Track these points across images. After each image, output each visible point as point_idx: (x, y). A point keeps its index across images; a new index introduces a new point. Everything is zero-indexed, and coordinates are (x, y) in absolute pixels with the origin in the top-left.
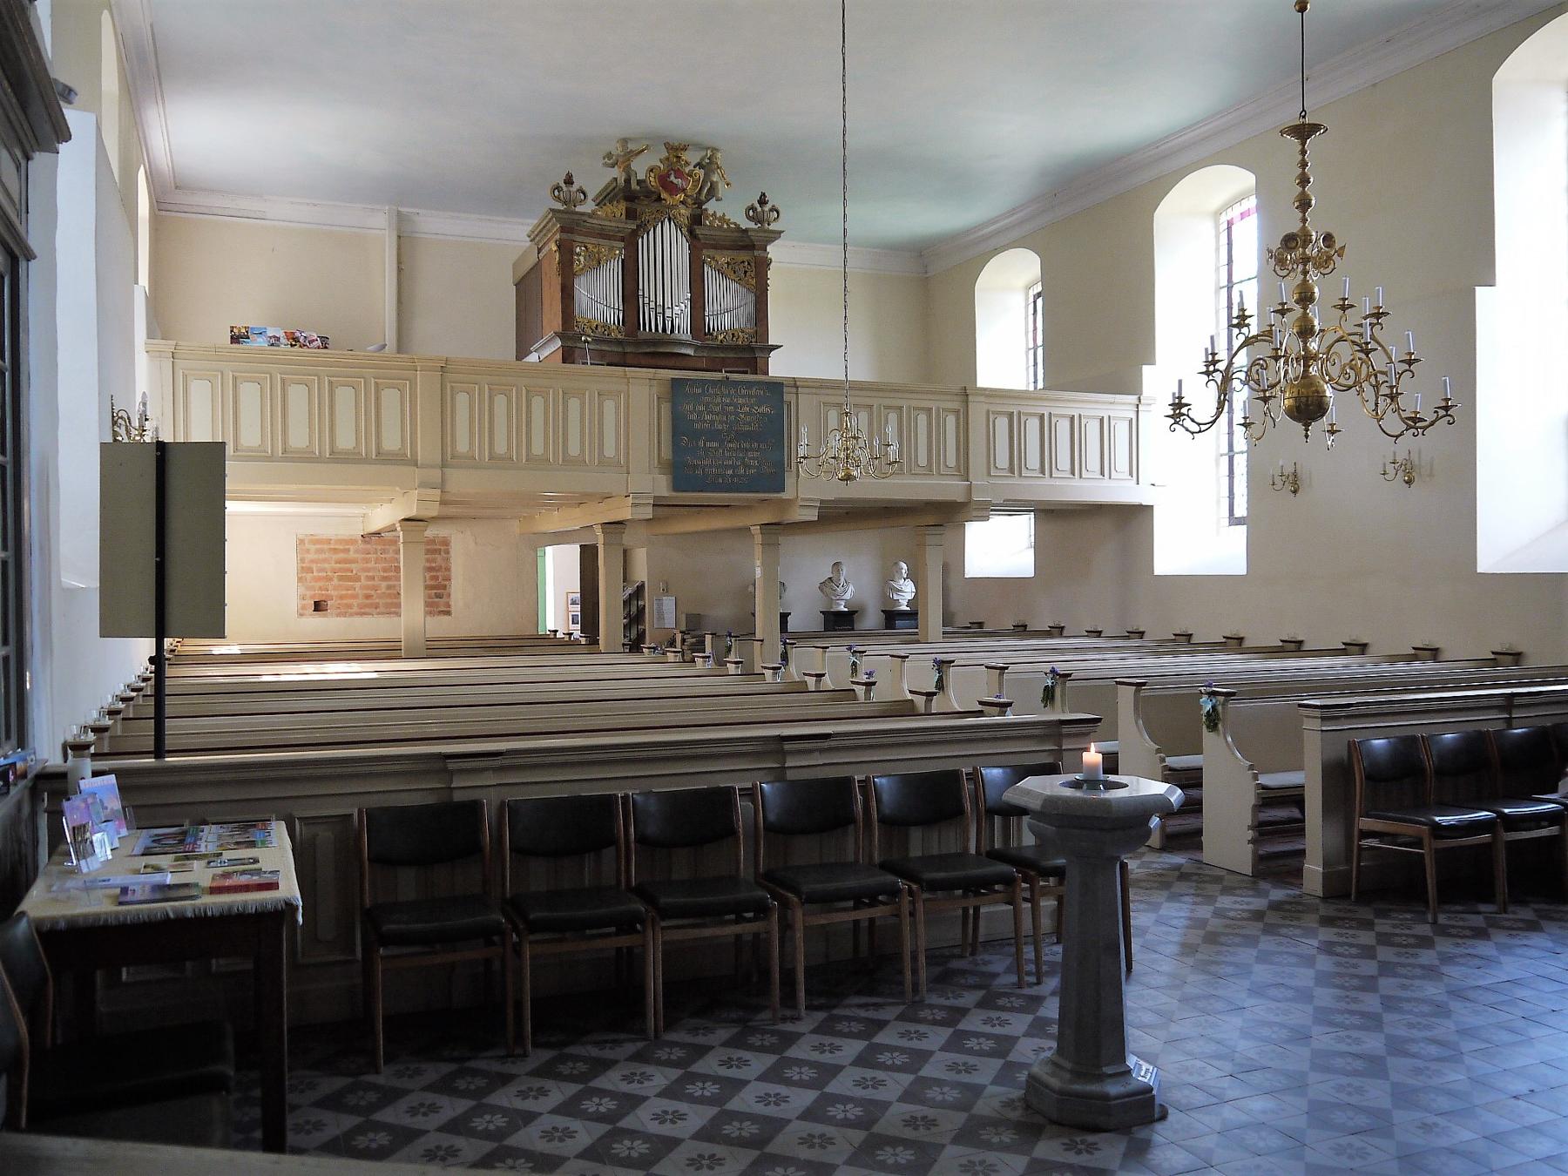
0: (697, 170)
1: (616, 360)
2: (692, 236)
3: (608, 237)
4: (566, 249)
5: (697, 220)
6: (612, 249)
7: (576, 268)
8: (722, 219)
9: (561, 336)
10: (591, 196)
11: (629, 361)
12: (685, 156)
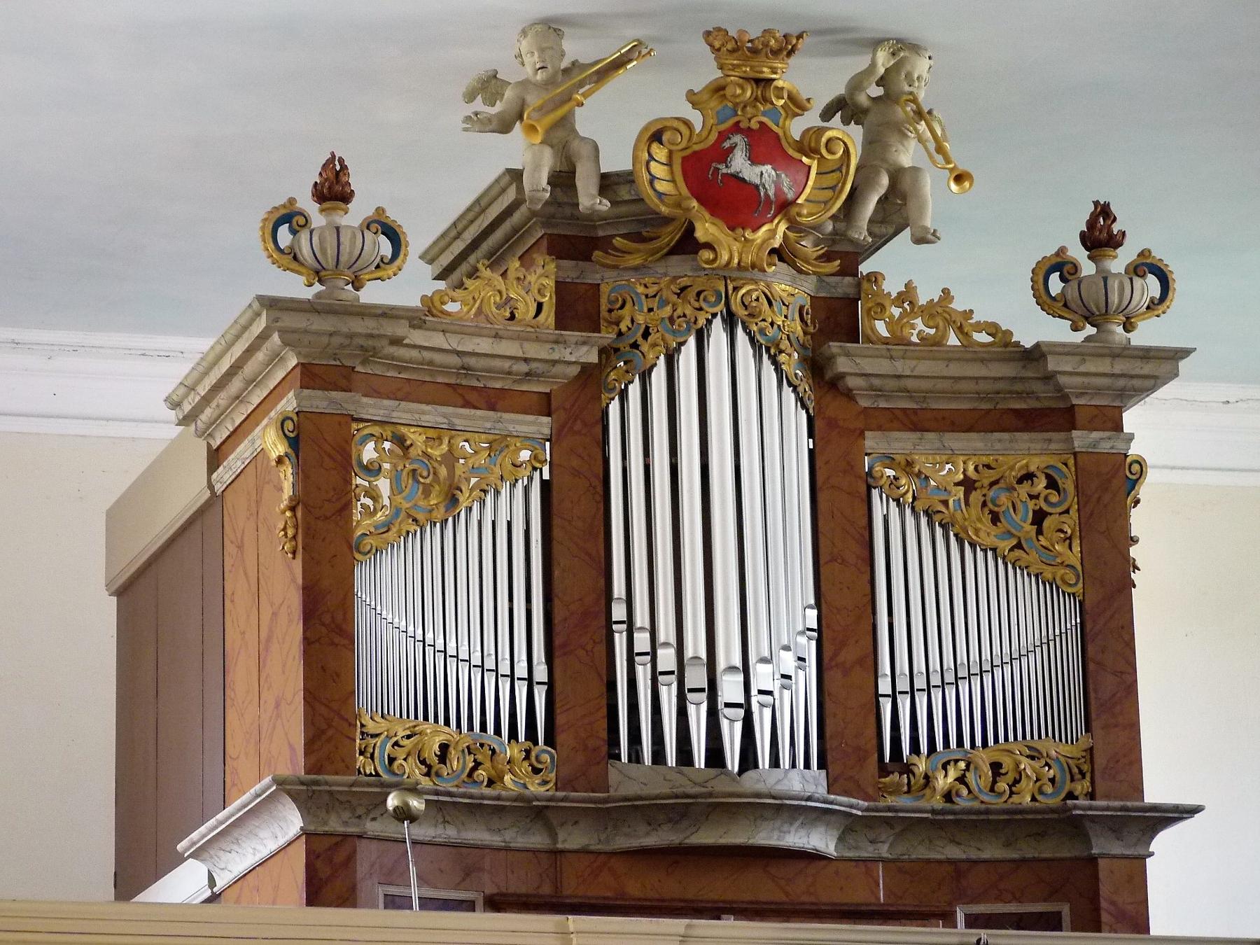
0: (835, 127)
1: (517, 885)
2: (822, 386)
3: (493, 400)
4: (321, 452)
5: (837, 318)
6: (499, 444)
7: (361, 523)
8: (940, 311)
9: (306, 794)
10: (418, 239)
11: (572, 889)
12: (792, 76)
